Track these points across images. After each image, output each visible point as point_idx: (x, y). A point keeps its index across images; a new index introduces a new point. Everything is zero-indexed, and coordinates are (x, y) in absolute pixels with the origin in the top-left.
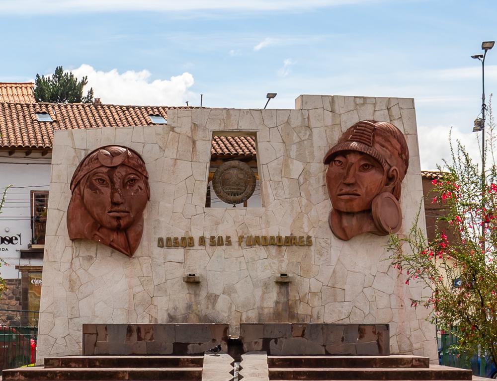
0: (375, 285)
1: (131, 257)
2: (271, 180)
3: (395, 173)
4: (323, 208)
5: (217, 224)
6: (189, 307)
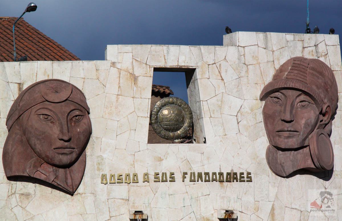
2: (211, 117)
5: (160, 160)
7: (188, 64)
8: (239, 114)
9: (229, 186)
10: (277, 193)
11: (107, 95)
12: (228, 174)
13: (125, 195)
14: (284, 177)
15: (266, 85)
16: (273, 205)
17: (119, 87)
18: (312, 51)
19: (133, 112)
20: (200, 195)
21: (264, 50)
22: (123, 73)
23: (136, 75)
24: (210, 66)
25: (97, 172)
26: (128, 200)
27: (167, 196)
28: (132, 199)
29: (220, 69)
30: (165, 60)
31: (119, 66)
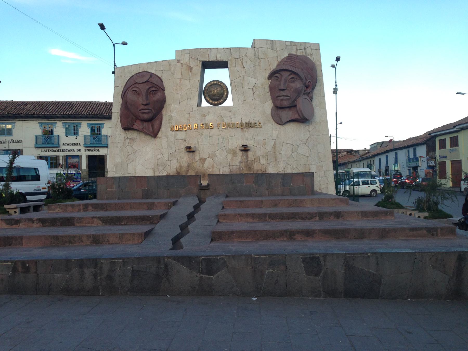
0: (299, 151)
1: (155, 138)
2: (236, 90)
3: (310, 83)
4: (269, 106)
5: (205, 116)
6: (189, 165)
7: (222, 59)
8: (254, 88)
9: (247, 130)
10: (278, 134)
11: (175, 79)
12: (246, 123)
13: (184, 137)
14: (282, 125)
15: (272, 70)
16: (275, 141)
17: (182, 74)
18: (302, 52)
19: (189, 88)
20: (228, 136)
21: (271, 50)
22: (184, 66)
23: (191, 67)
24: (236, 60)
25: (168, 124)
26: (186, 140)
27: (209, 137)
28: (188, 140)
29: (243, 61)
30: (209, 57)
31: (182, 62)
